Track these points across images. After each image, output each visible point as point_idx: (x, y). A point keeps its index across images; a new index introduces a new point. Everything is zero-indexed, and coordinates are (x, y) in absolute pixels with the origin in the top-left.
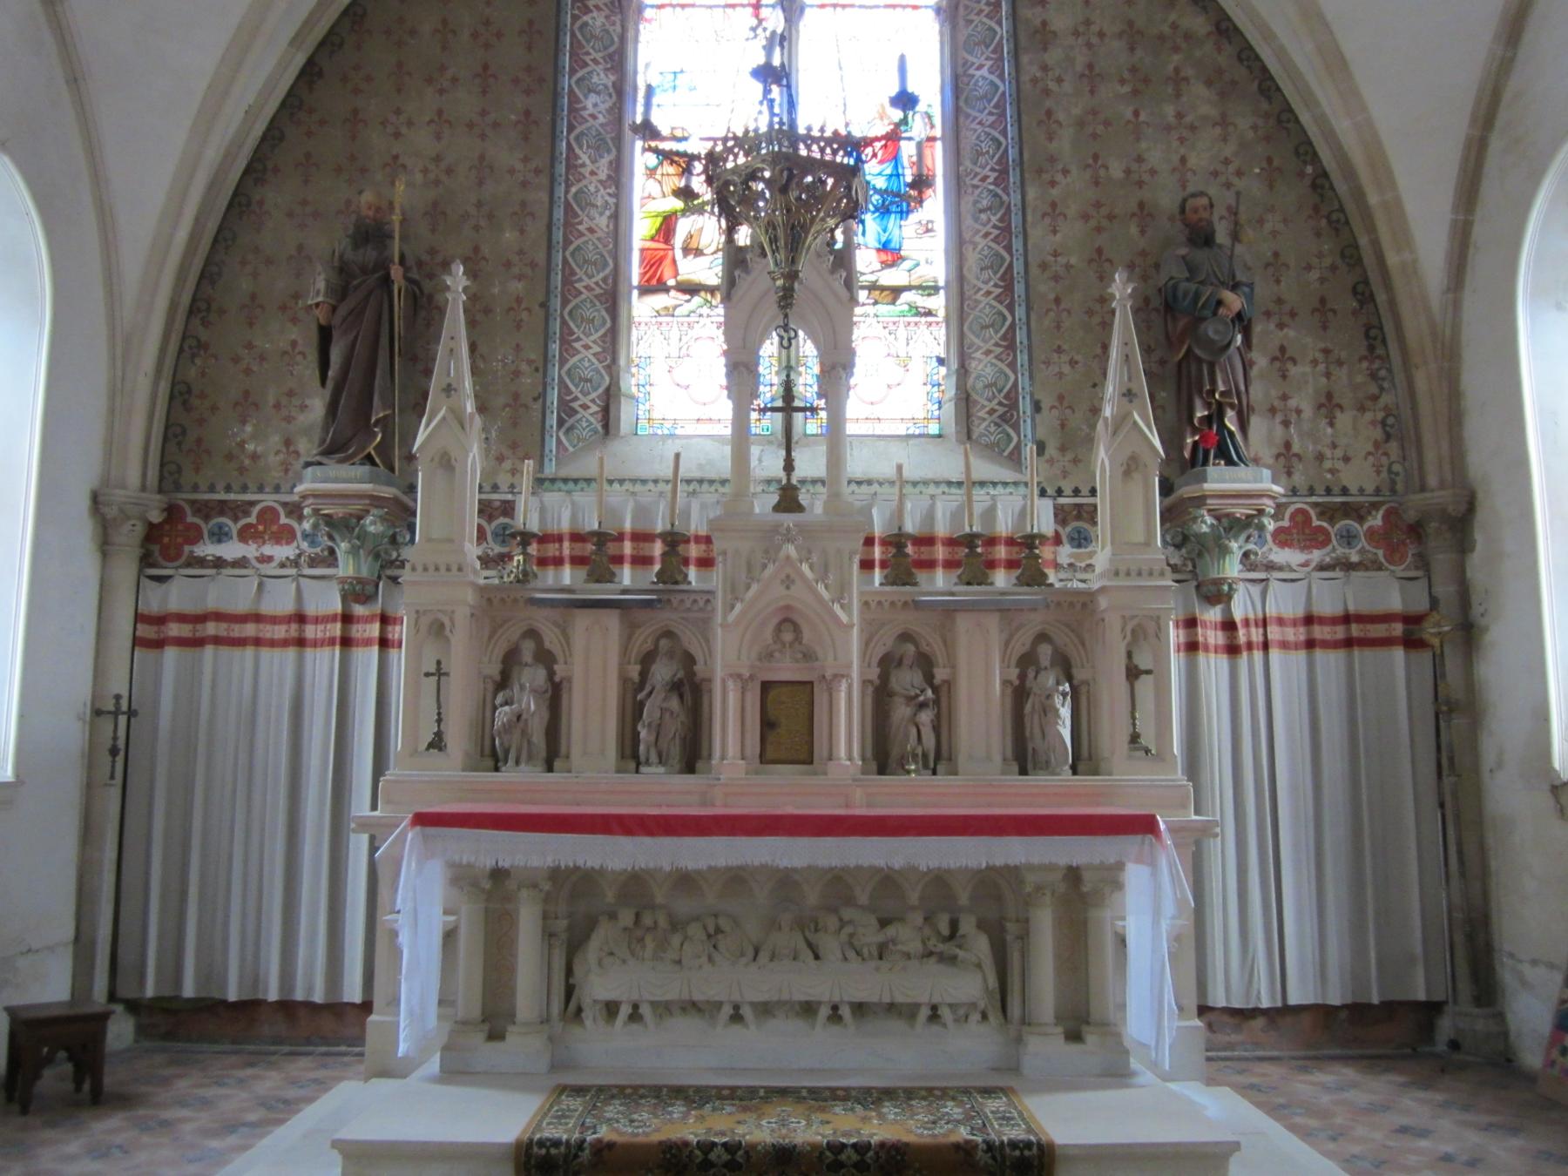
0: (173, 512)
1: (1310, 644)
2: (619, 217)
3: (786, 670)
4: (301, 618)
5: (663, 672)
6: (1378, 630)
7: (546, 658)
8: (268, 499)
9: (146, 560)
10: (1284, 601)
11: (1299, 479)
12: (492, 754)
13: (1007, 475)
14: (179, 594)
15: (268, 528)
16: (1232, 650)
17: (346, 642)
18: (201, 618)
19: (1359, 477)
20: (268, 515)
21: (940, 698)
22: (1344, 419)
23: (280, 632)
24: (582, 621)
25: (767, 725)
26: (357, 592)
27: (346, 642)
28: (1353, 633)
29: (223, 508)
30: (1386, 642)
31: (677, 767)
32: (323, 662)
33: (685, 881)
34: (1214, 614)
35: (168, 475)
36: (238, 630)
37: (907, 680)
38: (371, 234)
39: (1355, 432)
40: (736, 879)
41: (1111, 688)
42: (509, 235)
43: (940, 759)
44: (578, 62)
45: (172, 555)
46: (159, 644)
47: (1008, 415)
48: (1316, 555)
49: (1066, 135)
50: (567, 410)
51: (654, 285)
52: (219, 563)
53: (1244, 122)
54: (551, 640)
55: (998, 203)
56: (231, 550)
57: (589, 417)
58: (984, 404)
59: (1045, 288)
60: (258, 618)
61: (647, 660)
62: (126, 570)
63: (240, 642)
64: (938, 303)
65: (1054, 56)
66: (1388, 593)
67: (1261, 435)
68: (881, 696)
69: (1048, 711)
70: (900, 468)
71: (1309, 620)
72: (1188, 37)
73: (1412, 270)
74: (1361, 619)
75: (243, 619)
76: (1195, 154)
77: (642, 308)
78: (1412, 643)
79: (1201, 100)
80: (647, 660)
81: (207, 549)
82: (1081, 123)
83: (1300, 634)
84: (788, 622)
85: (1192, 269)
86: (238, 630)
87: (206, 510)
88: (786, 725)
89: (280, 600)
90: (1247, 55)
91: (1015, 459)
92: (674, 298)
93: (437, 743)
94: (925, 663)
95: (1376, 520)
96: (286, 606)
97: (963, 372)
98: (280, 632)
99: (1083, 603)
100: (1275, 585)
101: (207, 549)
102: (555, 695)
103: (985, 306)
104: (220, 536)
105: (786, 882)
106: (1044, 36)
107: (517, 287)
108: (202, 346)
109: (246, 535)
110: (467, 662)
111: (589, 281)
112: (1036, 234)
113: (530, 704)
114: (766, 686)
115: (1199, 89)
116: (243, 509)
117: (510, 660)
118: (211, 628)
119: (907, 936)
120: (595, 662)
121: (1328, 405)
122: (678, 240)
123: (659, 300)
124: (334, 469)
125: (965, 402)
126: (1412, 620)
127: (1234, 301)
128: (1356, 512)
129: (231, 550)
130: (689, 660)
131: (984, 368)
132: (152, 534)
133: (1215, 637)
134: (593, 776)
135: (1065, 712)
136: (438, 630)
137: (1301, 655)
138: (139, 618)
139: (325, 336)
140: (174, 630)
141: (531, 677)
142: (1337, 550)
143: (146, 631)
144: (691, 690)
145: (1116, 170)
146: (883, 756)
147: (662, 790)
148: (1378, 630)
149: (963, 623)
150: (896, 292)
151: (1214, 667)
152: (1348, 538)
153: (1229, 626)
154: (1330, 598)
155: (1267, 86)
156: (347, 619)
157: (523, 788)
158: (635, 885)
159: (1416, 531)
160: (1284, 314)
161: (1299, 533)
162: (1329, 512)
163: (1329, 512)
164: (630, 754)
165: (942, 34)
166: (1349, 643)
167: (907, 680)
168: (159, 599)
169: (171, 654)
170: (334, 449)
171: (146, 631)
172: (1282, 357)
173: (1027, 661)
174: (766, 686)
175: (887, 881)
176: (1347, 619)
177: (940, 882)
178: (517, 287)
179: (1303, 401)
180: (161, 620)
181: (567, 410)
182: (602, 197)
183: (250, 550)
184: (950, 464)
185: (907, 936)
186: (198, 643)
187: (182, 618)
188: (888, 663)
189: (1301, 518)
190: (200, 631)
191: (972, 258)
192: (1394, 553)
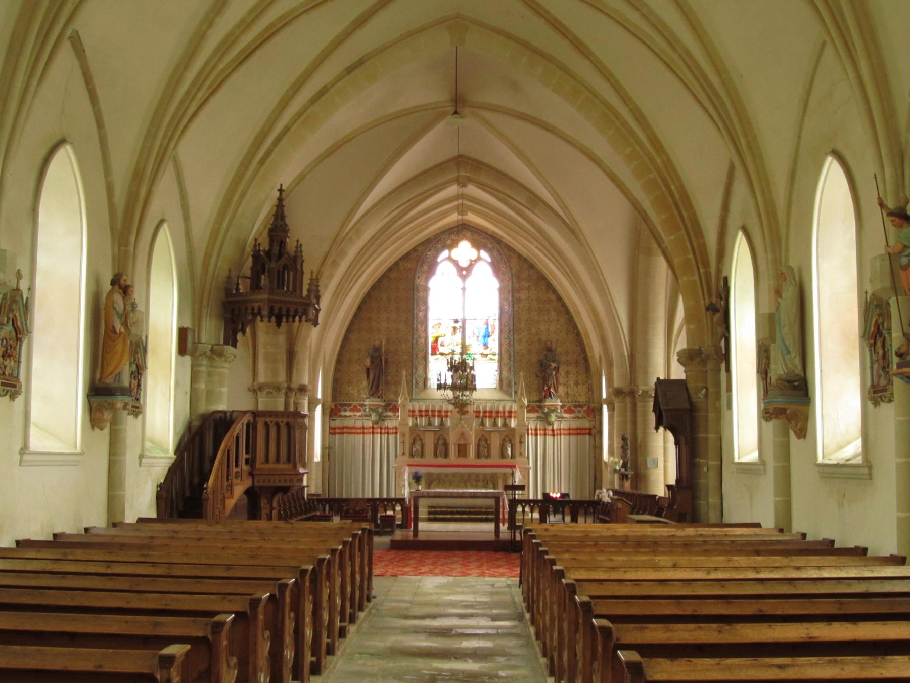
0: (336, 406)
1: (570, 434)
2: (426, 339)
3: (462, 442)
4: (363, 428)
5: (441, 442)
6: (584, 431)
7: (421, 439)
8: (355, 403)
9: (330, 416)
10: (564, 425)
11: (570, 399)
12: (412, 456)
13: (508, 398)
14: (337, 423)
15: (355, 409)
16: (553, 435)
17: (373, 433)
18: (343, 428)
19: (582, 399)
20: (355, 406)
21: (489, 447)
22: (580, 387)
23: (359, 431)
24: (427, 434)
25: (459, 451)
26: (376, 423)
27: (373, 433)
28: (579, 432)
29: (346, 405)
30: (585, 434)
31: (246, 516)
32: (368, 437)
33: (446, 475)
34: (550, 428)
35: (334, 398)
36: (350, 430)
37: (483, 443)
38: (377, 349)
39: (582, 389)
40: (454, 475)
41: (517, 445)
42: (404, 346)
43: (488, 456)
44: (418, 305)
45: (336, 415)
46: (335, 433)
47: (509, 385)
48: (572, 415)
49: (523, 323)
50: (417, 383)
51: (434, 353)
52: (346, 416)
53: (562, 320)
54: (422, 436)
55: (508, 338)
56: (348, 414)
57: (421, 384)
58: (505, 382)
59: (518, 358)
60: (355, 428)
61: (438, 440)
62: (327, 418)
63: (352, 433)
64: (496, 357)
65: (521, 305)
66: (586, 424)
67: (561, 390)
68: (478, 446)
69: (506, 449)
70: (374, 597)
71: (570, 429)
72: (551, 300)
73: (593, 356)
74: (580, 429)
75: (352, 428)
76: (551, 330)
77: (431, 358)
78: (590, 434)
79: (553, 315)
80: (438, 440)
81: (343, 414)
82: (526, 320)
83: (566, 432)
84: (462, 434)
85: (546, 356)
86: (350, 430)
87: (342, 405)
88: (462, 450)
89: (359, 424)
90: (564, 305)
91: (510, 395)
92: (439, 356)
93: (404, 454)
94: (486, 440)
95: (585, 408)
96: (361, 426)
97: (501, 374)
98: (359, 431)
99: (514, 429)
100: (561, 421)
101: (343, 414)
102: (422, 446)
103: (505, 360)
104: (345, 411)
105: (462, 475)
106: (519, 300)
107: (405, 357)
108: (339, 370)
109: (351, 410)
110: (408, 440)
111: (421, 355)
112: (516, 345)
113: (419, 447)
114: (459, 445)
115: (553, 313)
116: (350, 405)
117: (414, 440)
118: (345, 430)
119: (480, 483)
120: (429, 441)
121: (577, 383)
122: (439, 343)
123: (435, 357)
124: (372, 399)
125: (501, 381)
126: (590, 429)
127: (553, 365)
128: (581, 406)
129: (348, 414)
130: (445, 440)
131: (505, 374)
132: (332, 411)
133: (550, 432)
134: (429, 458)
135: (509, 449)
136: (404, 435)
137: (567, 437)
138: (330, 428)
139: (368, 370)
140: (337, 430)
141: (418, 443)
142: (577, 414)
143: (332, 431)
144: (446, 445)
145: (534, 331)
146: (478, 456)
147: (441, 461)
148: (584, 431)
149: (493, 434)
150: (487, 355)
151: (549, 439)
152: (579, 412)
153: (553, 430)
154: (574, 424)
155: (567, 311)
156: (373, 428)
157: (417, 460)
158: (439, 475)
159: (593, 410)
160: (568, 363)
161: (569, 411)
162: (575, 406)
163: (575, 406)
164: (436, 455)
165: (501, 291)
166: (578, 434)
167: (483, 443)
168: (333, 424)
169: (337, 436)
170: (372, 395)
171: (332, 431)
172: (567, 373)
173: (504, 440)
174: (459, 445)
175: (477, 475)
176: (577, 429)
177: (485, 475)
178: (405, 357)
179: (571, 383)
180: (335, 428)
181: (417, 383)
182: (423, 335)
183: (352, 414)
184: (498, 395)
185: (480, 483)
186: (343, 433)
187: (339, 428)
188: (480, 440)
189: (570, 407)
190: (343, 431)
191: (503, 349)
192: (588, 415)
